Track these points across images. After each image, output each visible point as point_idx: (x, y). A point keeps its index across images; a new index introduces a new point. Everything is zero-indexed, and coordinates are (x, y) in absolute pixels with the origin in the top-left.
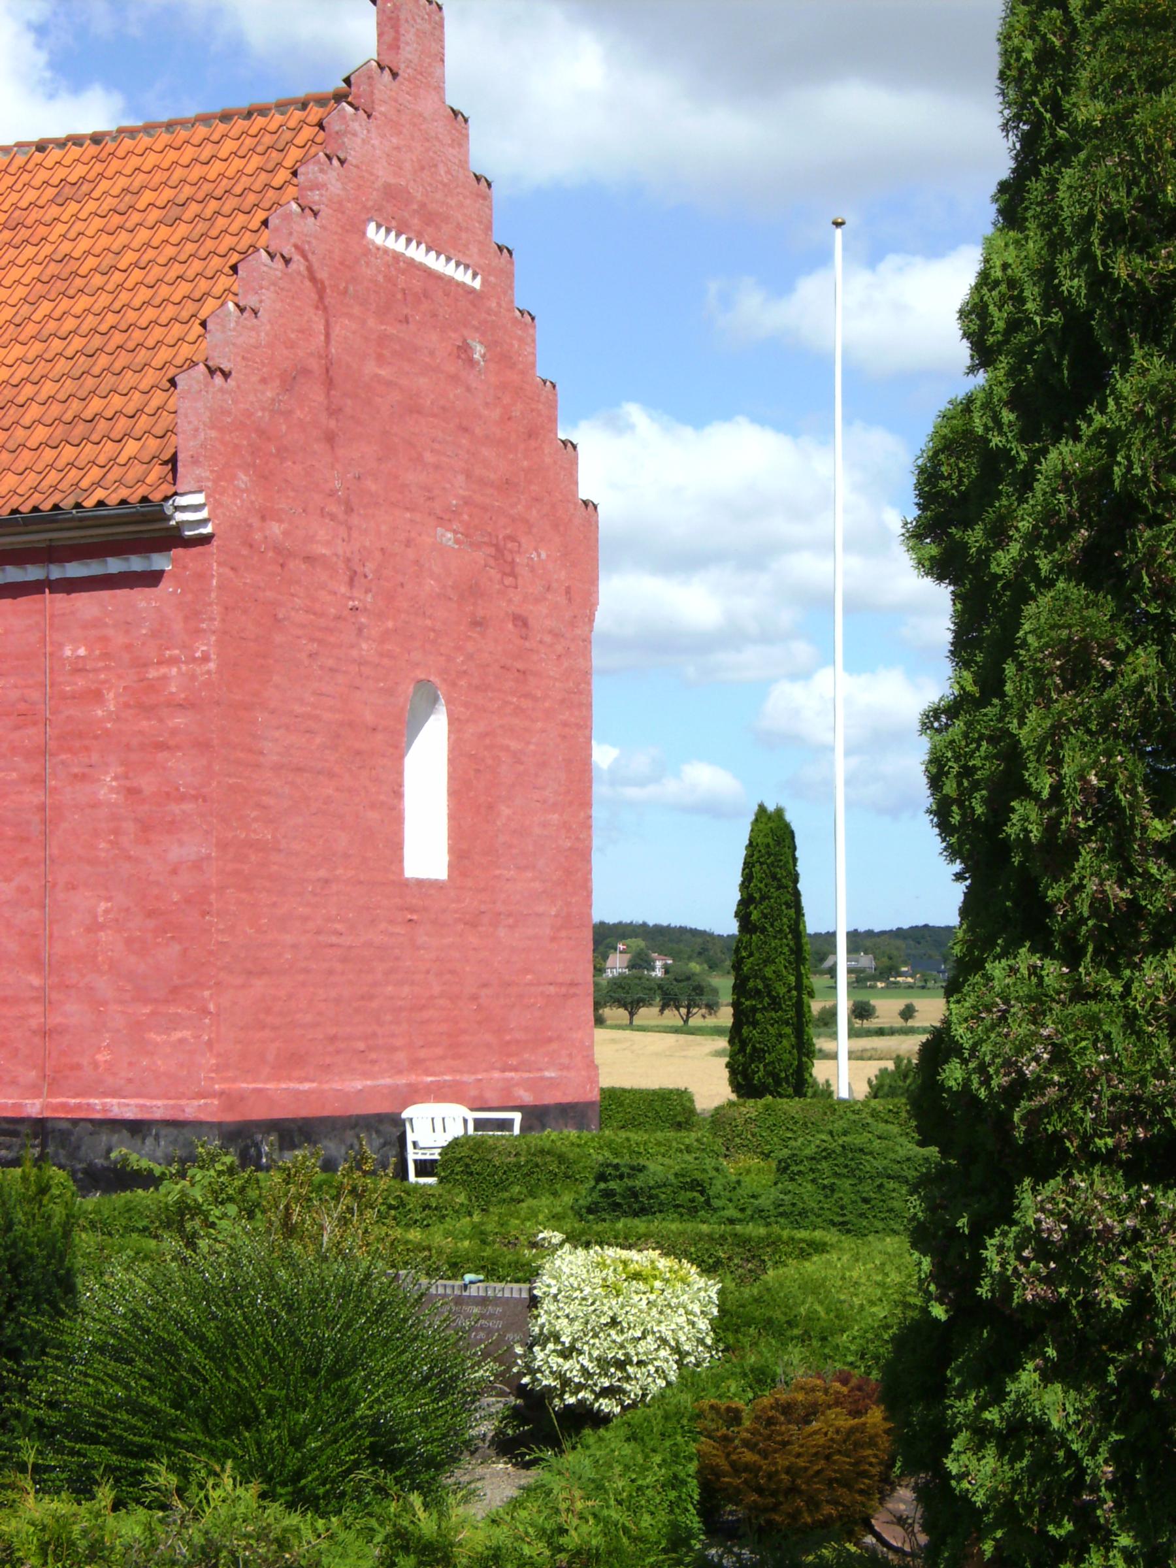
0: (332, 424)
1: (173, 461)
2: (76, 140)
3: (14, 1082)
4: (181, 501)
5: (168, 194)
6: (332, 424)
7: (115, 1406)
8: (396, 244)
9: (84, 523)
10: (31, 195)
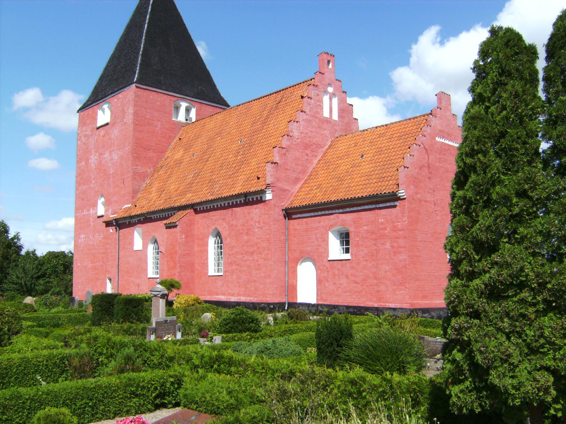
0: (430, 175)
1: (398, 184)
2: (383, 126)
3: (372, 300)
4: (400, 192)
5: (399, 134)
6: (430, 175)
7: (356, 356)
8: (442, 140)
9: (382, 197)
10: (375, 136)
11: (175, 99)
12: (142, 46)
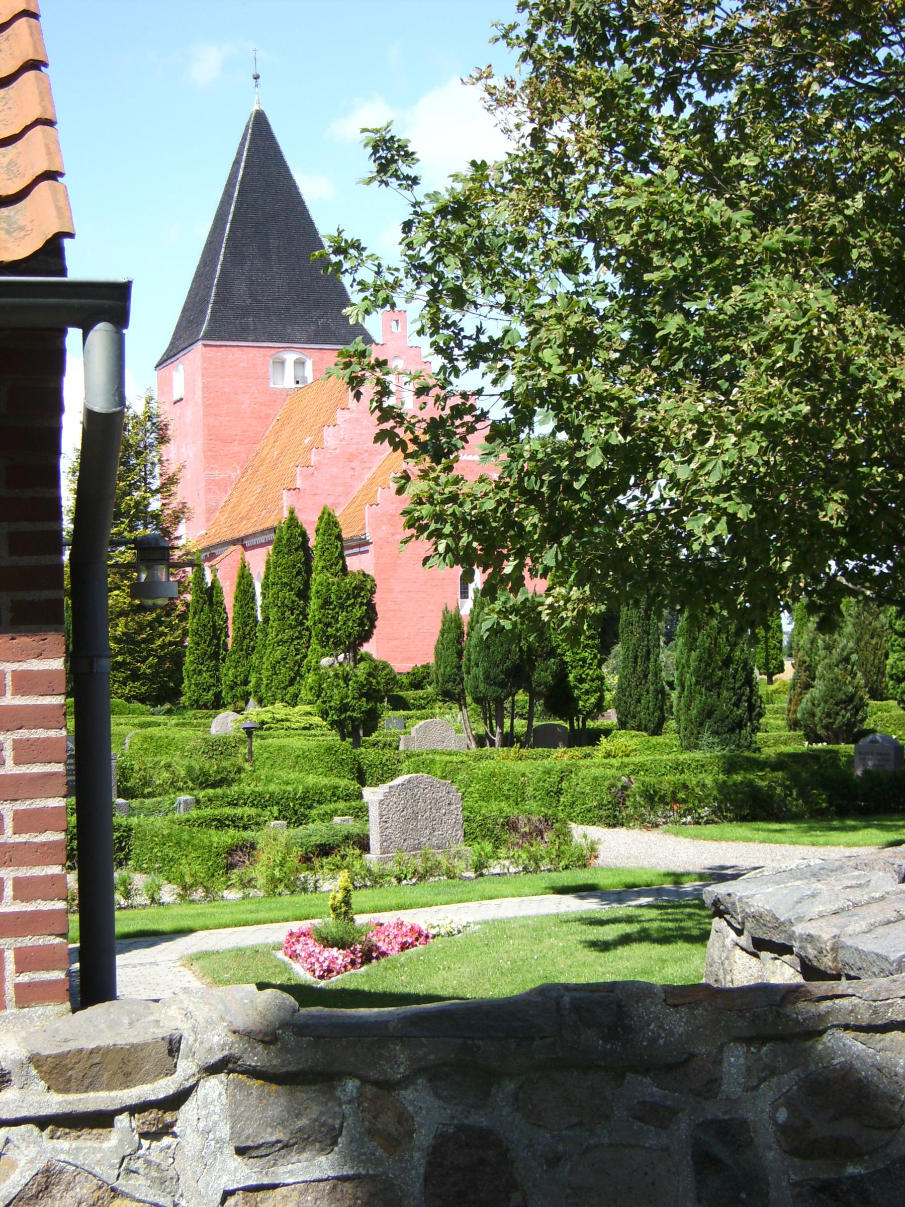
11: (273, 351)
12: (219, 267)
